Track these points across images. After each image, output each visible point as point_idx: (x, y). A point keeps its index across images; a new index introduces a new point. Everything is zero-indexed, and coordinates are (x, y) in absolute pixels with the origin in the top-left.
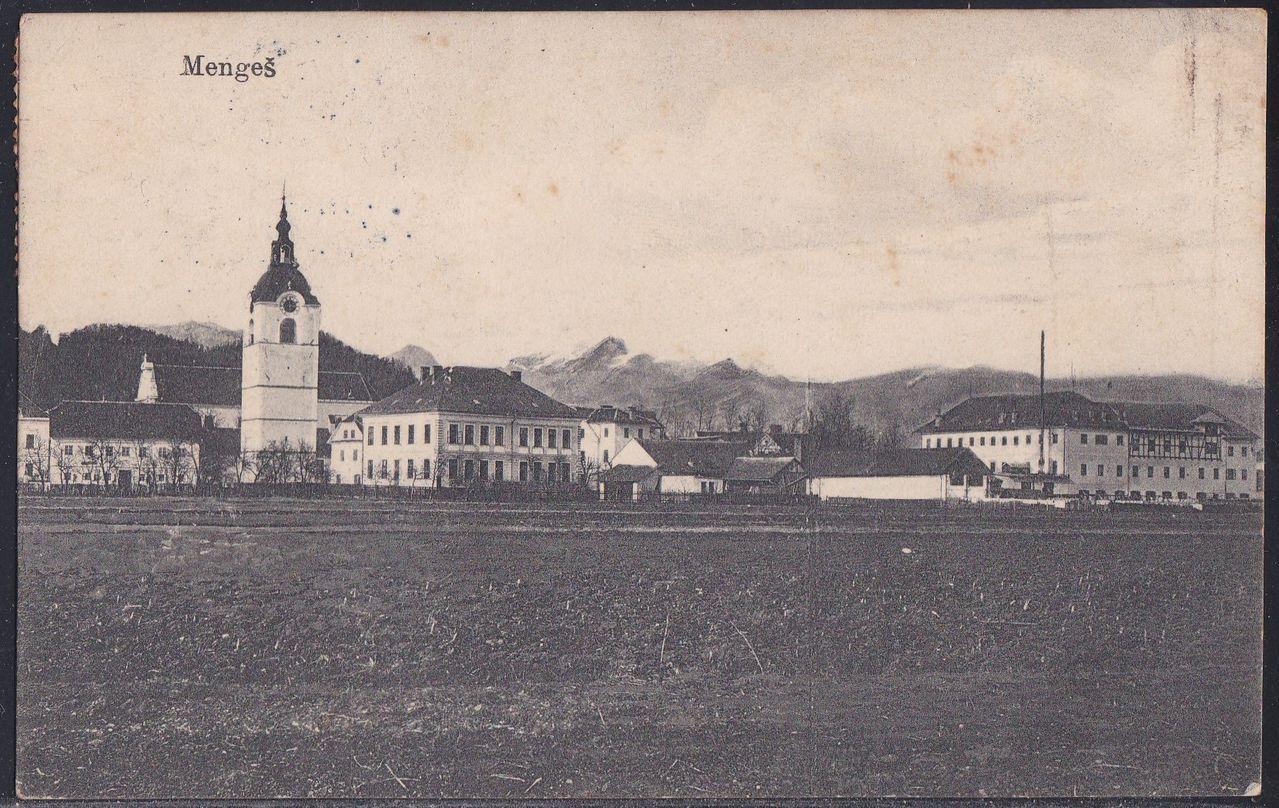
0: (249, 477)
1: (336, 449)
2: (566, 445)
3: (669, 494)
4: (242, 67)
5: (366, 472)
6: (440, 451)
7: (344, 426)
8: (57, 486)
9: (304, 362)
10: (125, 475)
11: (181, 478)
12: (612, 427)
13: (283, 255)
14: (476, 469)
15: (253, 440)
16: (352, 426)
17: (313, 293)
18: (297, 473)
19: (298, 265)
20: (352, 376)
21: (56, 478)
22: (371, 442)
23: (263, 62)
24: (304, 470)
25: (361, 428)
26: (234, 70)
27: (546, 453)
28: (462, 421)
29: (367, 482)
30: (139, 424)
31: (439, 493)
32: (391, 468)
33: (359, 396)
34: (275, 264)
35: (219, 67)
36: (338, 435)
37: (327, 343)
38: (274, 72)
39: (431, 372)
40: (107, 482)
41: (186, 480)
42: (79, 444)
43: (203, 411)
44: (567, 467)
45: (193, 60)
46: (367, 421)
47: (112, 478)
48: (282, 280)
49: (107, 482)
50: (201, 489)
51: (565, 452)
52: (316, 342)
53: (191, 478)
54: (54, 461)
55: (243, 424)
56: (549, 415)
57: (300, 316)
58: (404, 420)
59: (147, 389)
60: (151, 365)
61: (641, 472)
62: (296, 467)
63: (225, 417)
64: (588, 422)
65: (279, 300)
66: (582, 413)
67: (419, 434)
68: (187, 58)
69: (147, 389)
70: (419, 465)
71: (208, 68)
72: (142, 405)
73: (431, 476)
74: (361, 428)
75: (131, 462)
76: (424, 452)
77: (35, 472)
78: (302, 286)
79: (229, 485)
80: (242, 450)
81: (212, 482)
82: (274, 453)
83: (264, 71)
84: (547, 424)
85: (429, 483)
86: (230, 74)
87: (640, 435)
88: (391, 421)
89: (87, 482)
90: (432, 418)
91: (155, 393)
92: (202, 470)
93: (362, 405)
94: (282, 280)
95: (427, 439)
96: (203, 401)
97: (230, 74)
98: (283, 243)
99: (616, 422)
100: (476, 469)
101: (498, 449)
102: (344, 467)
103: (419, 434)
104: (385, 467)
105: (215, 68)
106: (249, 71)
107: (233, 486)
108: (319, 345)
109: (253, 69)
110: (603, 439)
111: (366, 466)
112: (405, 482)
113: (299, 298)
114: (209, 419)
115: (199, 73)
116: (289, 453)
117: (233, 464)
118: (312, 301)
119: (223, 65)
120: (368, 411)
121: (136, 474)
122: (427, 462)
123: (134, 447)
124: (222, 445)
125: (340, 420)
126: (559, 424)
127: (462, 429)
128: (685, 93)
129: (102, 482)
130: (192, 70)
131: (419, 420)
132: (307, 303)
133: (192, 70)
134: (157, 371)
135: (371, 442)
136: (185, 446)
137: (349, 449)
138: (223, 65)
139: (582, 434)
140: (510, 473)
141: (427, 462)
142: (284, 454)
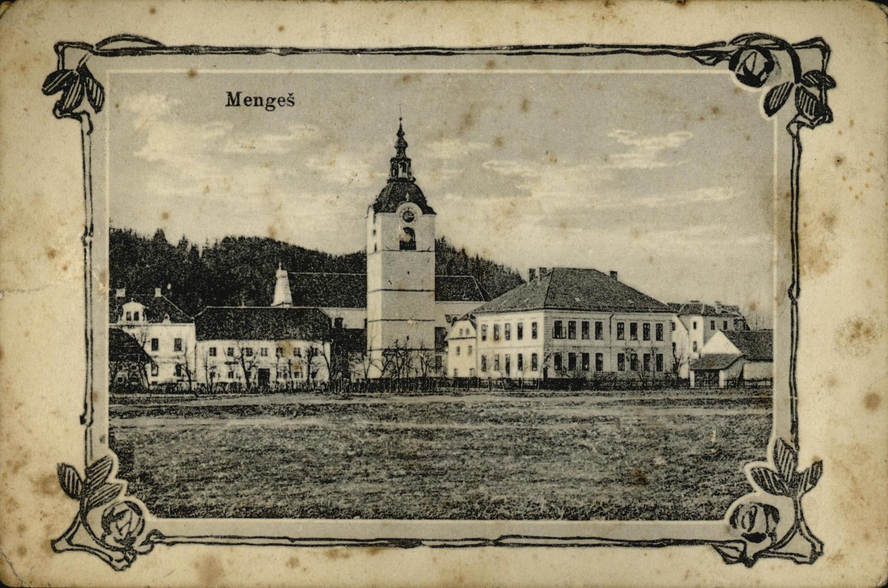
0: (375, 373)
1: (452, 346)
2: (659, 338)
3: (753, 380)
4: (270, 100)
5: (480, 365)
6: (547, 346)
7: (460, 325)
8: (203, 385)
9: (422, 269)
10: (264, 374)
11: (314, 375)
12: (699, 320)
13: (400, 170)
14: (579, 360)
15: (376, 340)
16: (467, 324)
17: (429, 204)
18: (416, 369)
19: (414, 179)
20: (465, 278)
21: (201, 376)
22: (484, 338)
23: (286, 96)
24: (424, 366)
25: (475, 326)
26: (265, 102)
27: (642, 347)
28: (566, 318)
29: (481, 375)
30: (277, 325)
31: (545, 384)
32: (503, 363)
33: (473, 297)
34: (394, 180)
35: (253, 100)
36: (454, 332)
37: (441, 247)
38: (293, 103)
39: (537, 274)
40: (248, 381)
41: (318, 378)
42: (222, 345)
43: (333, 313)
44: (660, 358)
45: (234, 95)
46: (481, 320)
47: (253, 376)
48: (401, 192)
49: (248, 381)
50: (331, 387)
51: (658, 344)
52: (433, 249)
53: (324, 375)
54: (200, 363)
55: (369, 325)
56: (645, 310)
57: (421, 222)
58: (513, 319)
59: (282, 295)
60: (285, 273)
61: (729, 362)
62: (416, 363)
63: (351, 318)
64: (678, 316)
65: (399, 210)
66: (673, 308)
67: (527, 331)
68: (230, 94)
69: (282, 295)
70: (527, 359)
71: (245, 101)
72: (277, 310)
73: (539, 368)
74: (475, 326)
75: (269, 361)
76: (532, 346)
77: (183, 372)
78: (419, 199)
79: (358, 380)
80: (368, 348)
81: (341, 382)
82: (396, 350)
83: (287, 102)
84: (639, 318)
85: (538, 375)
86: (261, 105)
87: (725, 327)
88: (502, 320)
89: (230, 381)
90: (539, 317)
91: (289, 299)
92: (333, 370)
93: (477, 305)
94: (401, 192)
95: (534, 335)
96: (336, 304)
97: (261, 105)
98: (400, 161)
99: (703, 315)
100: (579, 360)
101: (598, 343)
102: (459, 363)
103: (527, 331)
104: (497, 361)
105: (251, 100)
106: (275, 103)
107: (360, 381)
108: (436, 251)
109: (279, 101)
110: (692, 330)
111: (480, 360)
112: (515, 374)
113: (416, 209)
114: (339, 321)
115: (238, 105)
116: (411, 350)
117: (361, 360)
118: (428, 210)
119: (256, 99)
120: (482, 311)
121: (273, 372)
122: (534, 355)
123: (271, 346)
124: (352, 342)
125: (455, 320)
126: (653, 319)
127: (565, 324)
128: (157, 498)
129: (243, 381)
130: (233, 102)
131: (527, 319)
132: (424, 213)
133: (233, 102)
134: (290, 277)
135: (484, 338)
136: (318, 345)
137: (464, 345)
138: (256, 99)
139: (673, 326)
140: (610, 365)
141: (534, 355)
142: (407, 351)
